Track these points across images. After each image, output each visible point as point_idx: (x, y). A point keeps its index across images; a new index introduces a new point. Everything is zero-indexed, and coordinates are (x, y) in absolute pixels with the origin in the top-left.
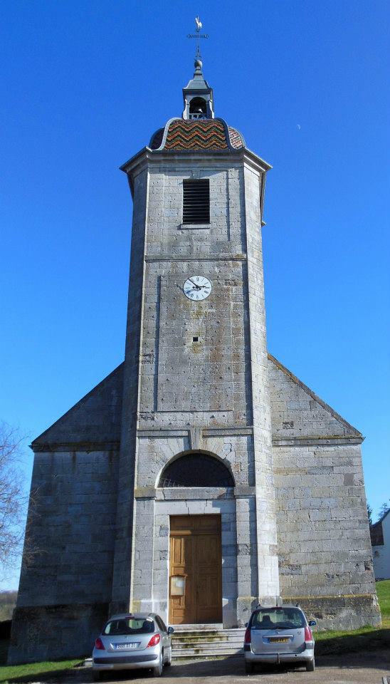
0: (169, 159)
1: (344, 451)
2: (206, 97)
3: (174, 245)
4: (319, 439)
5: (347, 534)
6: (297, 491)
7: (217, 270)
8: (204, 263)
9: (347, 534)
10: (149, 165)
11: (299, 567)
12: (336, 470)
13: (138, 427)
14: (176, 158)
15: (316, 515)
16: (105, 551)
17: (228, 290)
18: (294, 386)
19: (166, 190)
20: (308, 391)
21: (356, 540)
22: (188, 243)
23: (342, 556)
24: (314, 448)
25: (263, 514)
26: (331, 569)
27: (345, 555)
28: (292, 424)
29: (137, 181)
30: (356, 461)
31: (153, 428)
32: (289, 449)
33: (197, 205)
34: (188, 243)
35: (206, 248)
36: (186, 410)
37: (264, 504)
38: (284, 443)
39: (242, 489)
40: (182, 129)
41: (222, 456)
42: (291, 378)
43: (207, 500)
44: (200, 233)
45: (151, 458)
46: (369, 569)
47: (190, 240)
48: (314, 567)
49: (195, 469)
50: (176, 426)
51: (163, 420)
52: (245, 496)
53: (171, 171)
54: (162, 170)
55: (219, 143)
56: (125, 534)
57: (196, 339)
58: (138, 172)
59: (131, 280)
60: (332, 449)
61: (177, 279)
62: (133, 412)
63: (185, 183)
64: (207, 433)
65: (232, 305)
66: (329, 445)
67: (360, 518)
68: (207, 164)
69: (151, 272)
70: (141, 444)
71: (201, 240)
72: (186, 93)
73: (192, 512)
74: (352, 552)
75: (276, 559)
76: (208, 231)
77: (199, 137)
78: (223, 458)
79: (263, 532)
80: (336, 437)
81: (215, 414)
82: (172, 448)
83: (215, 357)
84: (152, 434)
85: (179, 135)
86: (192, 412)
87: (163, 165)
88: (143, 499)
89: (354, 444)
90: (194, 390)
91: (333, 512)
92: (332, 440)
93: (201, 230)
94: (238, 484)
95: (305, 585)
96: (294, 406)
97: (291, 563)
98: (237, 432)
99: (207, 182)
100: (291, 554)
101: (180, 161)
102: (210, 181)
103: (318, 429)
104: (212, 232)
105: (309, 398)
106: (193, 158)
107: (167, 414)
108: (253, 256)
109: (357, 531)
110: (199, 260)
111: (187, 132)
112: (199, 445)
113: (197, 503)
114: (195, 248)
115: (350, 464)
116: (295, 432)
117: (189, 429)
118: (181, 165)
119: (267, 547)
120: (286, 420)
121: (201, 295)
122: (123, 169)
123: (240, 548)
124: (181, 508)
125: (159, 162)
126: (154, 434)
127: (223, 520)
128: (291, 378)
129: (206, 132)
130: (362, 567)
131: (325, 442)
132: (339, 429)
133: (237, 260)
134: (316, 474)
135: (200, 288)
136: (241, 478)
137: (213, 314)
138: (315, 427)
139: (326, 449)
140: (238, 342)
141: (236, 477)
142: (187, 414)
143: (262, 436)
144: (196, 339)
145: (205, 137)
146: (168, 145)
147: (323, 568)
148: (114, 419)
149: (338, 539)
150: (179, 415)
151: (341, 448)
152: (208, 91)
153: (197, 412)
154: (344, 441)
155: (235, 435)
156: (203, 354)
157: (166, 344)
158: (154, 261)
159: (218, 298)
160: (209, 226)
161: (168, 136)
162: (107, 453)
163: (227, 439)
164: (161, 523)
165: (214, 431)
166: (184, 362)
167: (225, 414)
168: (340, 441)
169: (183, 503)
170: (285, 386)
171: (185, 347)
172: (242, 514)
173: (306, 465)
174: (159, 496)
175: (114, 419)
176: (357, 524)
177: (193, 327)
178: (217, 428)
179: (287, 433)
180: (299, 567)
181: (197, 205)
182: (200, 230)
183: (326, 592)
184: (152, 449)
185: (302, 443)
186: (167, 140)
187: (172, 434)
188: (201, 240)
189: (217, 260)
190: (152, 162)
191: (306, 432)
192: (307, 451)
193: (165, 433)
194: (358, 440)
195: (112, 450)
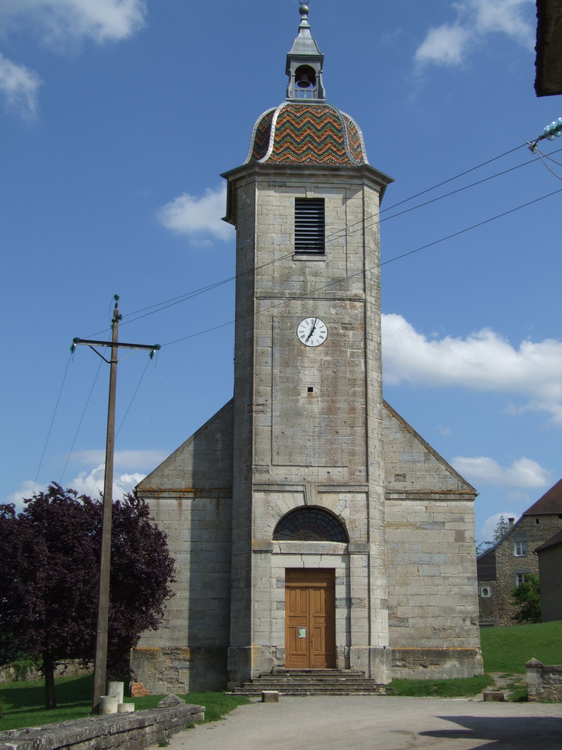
0: (280, 174)
1: (457, 506)
2: (316, 66)
3: (285, 279)
4: (432, 493)
5: (456, 590)
6: (406, 546)
7: (333, 311)
8: (319, 303)
9: (456, 590)
10: (258, 179)
11: (407, 619)
12: (448, 526)
13: (253, 481)
14: (289, 172)
15: (426, 570)
16: (214, 599)
17: (344, 335)
18: (408, 436)
19: (275, 208)
20: (423, 442)
21: (464, 596)
22: (302, 278)
23: (448, 611)
24: (426, 503)
25: (376, 570)
26: (437, 623)
27: (452, 610)
28: (404, 476)
29: (241, 194)
30: (468, 518)
31: (267, 482)
32: (400, 502)
33: (311, 235)
34: (302, 278)
35: (320, 284)
36: (301, 464)
37: (377, 561)
38: (395, 496)
39: (357, 545)
40: (292, 124)
41: (337, 512)
42: (405, 427)
43: (321, 555)
44: (315, 266)
45: (267, 510)
46: (474, 624)
47: (304, 273)
48: (421, 621)
49: (311, 523)
50: (291, 481)
51: (278, 474)
52: (359, 553)
53: (282, 187)
54: (272, 186)
55: (335, 147)
56: (242, 584)
57: (310, 390)
58: (243, 183)
59: (238, 316)
60: (444, 504)
61: (290, 321)
62: (248, 464)
63: (297, 200)
64: (322, 489)
65: (349, 352)
66: (441, 500)
67: (469, 575)
68: (322, 180)
69: (265, 311)
70: (258, 497)
71: (316, 274)
72: (290, 58)
73: (307, 566)
74: (458, 608)
75: (386, 612)
76: (323, 264)
77: (312, 138)
78: (338, 514)
79: (375, 587)
80: (449, 492)
81: (330, 469)
82: (288, 503)
83: (331, 410)
84: (266, 487)
85: (288, 135)
86: (307, 467)
87: (272, 178)
88: (261, 552)
89: (467, 500)
90: (309, 444)
91: (442, 568)
92: (445, 495)
93: (316, 263)
94: (352, 540)
95: (411, 637)
96: (407, 457)
97: (399, 615)
98: (351, 489)
99: (322, 200)
100: (399, 608)
101: (293, 175)
102: (326, 201)
103: (432, 482)
104: (327, 265)
105: (423, 449)
106: (307, 172)
107: (282, 468)
108: (371, 296)
109: (465, 587)
110: (314, 299)
111: (299, 130)
112: (315, 500)
113: (312, 557)
114: (309, 284)
115: (462, 520)
116: (407, 485)
117: (305, 483)
118: (293, 180)
119: (379, 602)
120: (398, 472)
121: (317, 339)
122: (225, 176)
123: (353, 601)
124: (296, 562)
125: (269, 175)
126: (268, 488)
127: (337, 575)
128: (405, 427)
129: (319, 131)
130: (468, 622)
131: (437, 496)
132: (452, 484)
133: (355, 300)
134: (426, 529)
135: (313, 332)
136: (356, 534)
137: (329, 362)
138: (428, 480)
139: (439, 503)
140: (354, 394)
141: (350, 533)
142: (302, 469)
143: (376, 493)
144: (310, 390)
145: (319, 137)
146: (277, 149)
147: (430, 622)
148: (220, 464)
149: (446, 595)
150: (294, 470)
151: (454, 503)
152: (319, 59)
153: (312, 466)
154: (458, 497)
155: (350, 492)
156: (317, 406)
157: (279, 394)
158: (265, 298)
159: (334, 343)
160: (324, 258)
161: (276, 135)
162: (214, 501)
163: (341, 496)
164: (278, 575)
165: (332, 487)
166: (299, 414)
167: (340, 469)
168: (453, 497)
169: (299, 557)
170: (399, 436)
171: (300, 397)
172: (356, 570)
173: (418, 519)
174: (276, 550)
175: (220, 464)
176: (466, 581)
177: (310, 376)
178: (332, 483)
179: (399, 486)
180: (407, 619)
181: (311, 235)
182: (315, 264)
183: (433, 644)
184: (267, 503)
185: (418, 496)
186: (275, 141)
187: (288, 488)
188: (316, 274)
189: (334, 299)
190: (260, 174)
191: (417, 486)
192: (419, 506)
193: (281, 487)
194: (473, 497)
195: (219, 498)
